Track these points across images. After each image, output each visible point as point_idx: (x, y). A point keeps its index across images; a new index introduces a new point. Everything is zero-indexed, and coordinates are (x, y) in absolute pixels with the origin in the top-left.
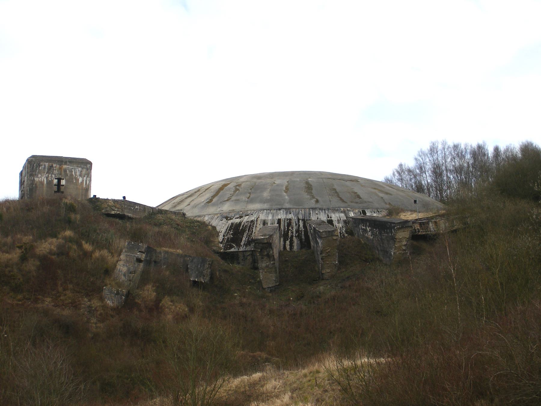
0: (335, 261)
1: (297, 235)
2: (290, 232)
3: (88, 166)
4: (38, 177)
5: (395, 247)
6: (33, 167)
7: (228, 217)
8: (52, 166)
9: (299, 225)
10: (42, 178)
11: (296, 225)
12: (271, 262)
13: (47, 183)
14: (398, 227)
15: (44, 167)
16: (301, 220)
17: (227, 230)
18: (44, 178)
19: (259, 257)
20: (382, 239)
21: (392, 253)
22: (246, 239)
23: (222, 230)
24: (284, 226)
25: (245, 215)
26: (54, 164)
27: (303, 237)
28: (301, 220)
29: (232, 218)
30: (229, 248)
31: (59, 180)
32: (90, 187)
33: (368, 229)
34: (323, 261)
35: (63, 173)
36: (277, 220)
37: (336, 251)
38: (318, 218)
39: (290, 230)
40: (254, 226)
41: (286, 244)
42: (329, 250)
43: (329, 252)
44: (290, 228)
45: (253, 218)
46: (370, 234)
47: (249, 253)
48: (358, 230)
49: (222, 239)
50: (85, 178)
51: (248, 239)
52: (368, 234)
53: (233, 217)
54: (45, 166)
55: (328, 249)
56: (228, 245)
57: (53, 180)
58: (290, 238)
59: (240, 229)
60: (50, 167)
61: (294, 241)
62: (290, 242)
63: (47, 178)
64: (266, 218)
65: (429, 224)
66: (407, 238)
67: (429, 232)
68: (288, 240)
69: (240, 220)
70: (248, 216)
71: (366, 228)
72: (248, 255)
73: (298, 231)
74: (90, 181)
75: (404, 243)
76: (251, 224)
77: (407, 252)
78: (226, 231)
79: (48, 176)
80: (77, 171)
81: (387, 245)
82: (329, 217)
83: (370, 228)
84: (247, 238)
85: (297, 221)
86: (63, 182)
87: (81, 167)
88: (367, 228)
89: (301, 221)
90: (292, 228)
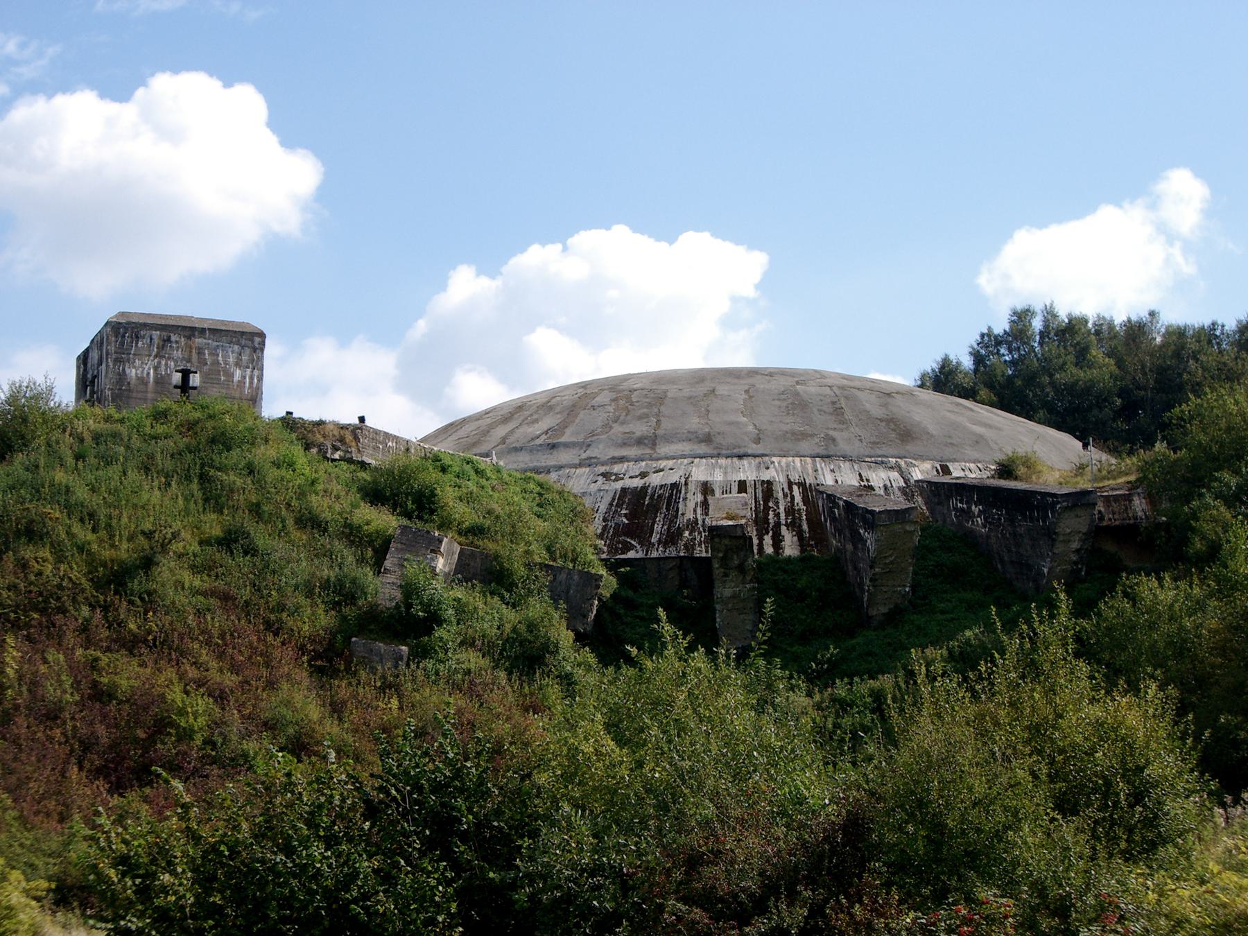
0: (905, 586)
1: (789, 521)
2: (770, 512)
3: (257, 340)
4: (134, 367)
5: (1054, 553)
6: (122, 344)
7: (611, 474)
8: (169, 340)
9: (793, 498)
10: (141, 369)
11: (785, 496)
12: (748, 586)
13: (157, 382)
14: (1065, 504)
15: (148, 341)
16: (795, 484)
17: (611, 504)
18: (149, 369)
19: (717, 572)
20: (1015, 535)
21: (1046, 570)
22: (662, 528)
23: (597, 505)
24: (755, 499)
25: (654, 470)
26: (172, 335)
27: (805, 527)
28: (795, 484)
29: (622, 476)
30: (621, 549)
31: (186, 374)
32: (260, 393)
33: (975, 509)
34: (873, 586)
35: (195, 356)
36: (737, 483)
37: (910, 561)
38: (837, 482)
39: (770, 508)
40: (682, 496)
41: (764, 542)
42: (891, 559)
43: (892, 563)
44: (771, 504)
45: (673, 478)
46: (980, 522)
47: (674, 563)
48: (945, 512)
49: (600, 527)
50: (249, 371)
51: (669, 529)
52: (973, 521)
53: (624, 475)
54: (151, 339)
55: (891, 556)
56: (618, 542)
57: (169, 376)
58: (772, 529)
59: (646, 503)
60: (164, 341)
61: (783, 537)
62: (773, 538)
63: (156, 368)
64: (709, 479)
65: (1131, 501)
66: (1083, 534)
67: (1130, 519)
68: (767, 533)
69: (642, 481)
70: (662, 473)
71: (969, 508)
72: (671, 569)
73: (790, 511)
74: (260, 378)
75: (1075, 545)
76: (672, 492)
77: (1081, 569)
78: (609, 509)
79: (159, 363)
80: (229, 356)
81: (1029, 548)
82: (864, 479)
83: (981, 507)
84: (665, 527)
85: (786, 486)
86: (195, 380)
87: (238, 343)
88: (973, 507)
89: (795, 488)
90: (777, 503)
